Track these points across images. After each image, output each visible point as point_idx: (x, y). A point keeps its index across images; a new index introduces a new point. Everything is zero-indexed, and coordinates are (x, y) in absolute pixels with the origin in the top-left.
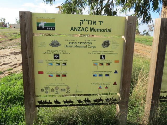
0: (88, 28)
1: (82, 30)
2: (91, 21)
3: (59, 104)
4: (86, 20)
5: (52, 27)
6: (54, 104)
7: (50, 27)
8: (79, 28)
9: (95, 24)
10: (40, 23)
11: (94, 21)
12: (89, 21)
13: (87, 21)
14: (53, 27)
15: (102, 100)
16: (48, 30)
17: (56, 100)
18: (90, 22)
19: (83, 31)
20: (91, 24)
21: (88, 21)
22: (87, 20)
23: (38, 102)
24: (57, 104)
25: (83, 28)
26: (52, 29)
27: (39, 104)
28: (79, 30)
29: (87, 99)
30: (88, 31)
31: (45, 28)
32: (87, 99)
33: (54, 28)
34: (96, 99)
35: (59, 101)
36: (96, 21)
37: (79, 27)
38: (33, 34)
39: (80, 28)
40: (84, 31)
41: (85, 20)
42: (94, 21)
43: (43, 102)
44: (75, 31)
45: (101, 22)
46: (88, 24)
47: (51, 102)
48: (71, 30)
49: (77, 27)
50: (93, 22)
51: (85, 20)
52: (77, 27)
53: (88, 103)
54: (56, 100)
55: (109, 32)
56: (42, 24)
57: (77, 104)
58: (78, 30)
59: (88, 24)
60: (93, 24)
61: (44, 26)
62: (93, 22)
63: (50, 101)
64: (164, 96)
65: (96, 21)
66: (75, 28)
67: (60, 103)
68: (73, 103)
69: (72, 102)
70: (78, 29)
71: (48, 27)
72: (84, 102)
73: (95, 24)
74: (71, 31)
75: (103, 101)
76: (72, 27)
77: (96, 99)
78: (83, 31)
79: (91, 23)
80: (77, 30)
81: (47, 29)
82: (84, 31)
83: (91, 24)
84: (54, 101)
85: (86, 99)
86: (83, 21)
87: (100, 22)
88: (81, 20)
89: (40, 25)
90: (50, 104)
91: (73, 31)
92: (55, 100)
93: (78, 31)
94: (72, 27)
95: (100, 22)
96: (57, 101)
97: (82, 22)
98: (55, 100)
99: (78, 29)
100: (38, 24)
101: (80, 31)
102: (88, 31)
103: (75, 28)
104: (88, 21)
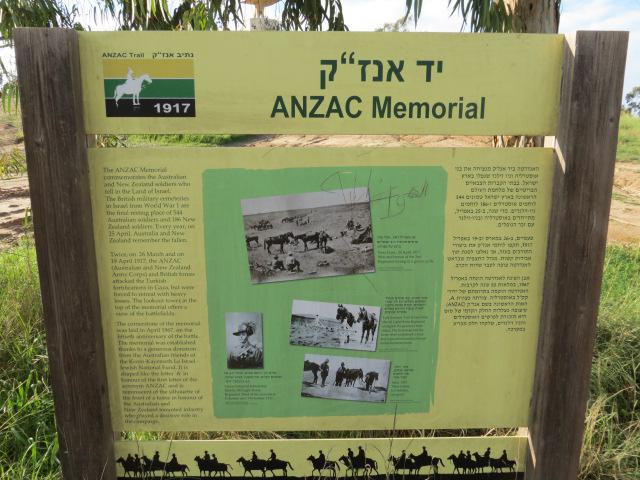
0: (359, 100)
1: (330, 110)
2: (376, 62)
3: (218, 475)
4: (352, 61)
5: (180, 102)
7: (172, 102)
9: (401, 79)
10: (123, 82)
12: (368, 62)
13: (356, 62)
16: (163, 114)
17: (207, 456)
20: (378, 79)
21: (360, 62)
22: (357, 58)
23: (121, 460)
24: (213, 474)
25: (334, 99)
26: (182, 108)
27: (127, 470)
29: (356, 453)
30: (359, 113)
32: (356, 453)
33: (188, 105)
34: (404, 455)
35: (219, 461)
36: (402, 63)
37: (312, 98)
39: (321, 99)
40: (341, 116)
41: (347, 57)
43: (473, 458)
44: (293, 115)
45: (429, 64)
47: (180, 462)
48: (275, 110)
49: (305, 98)
51: (344, 61)
52: (305, 98)
55: (475, 116)
56: (132, 88)
60: (389, 79)
62: (386, 68)
65: (402, 63)
66: (294, 100)
68: (288, 468)
69: (283, 465)
70: (311, 104)
71: (162, 102)
72: (342, 464)
73: (401, 79)
74: (273, 115)
76: (279, 99)
79: (376, 75)
80: (303, 114)
81: (153, 113)
82: (341, 116)
84: (197, 459)
86: (334, 63)
87: (425, 68)
88: (324, 62)
89: (119, 93)
91: (287, 115)
92: (202, 456)
93: (312, 115)
94: (279, 99)
95: (425, 68)
96: (212, 458)
97: (328, 69)
98: (202, 456)
99: (311, 104)
100: (110, 85)
101: (321, 116)
102: (359, 113)
103: (294, 100)
104: (360, 62)
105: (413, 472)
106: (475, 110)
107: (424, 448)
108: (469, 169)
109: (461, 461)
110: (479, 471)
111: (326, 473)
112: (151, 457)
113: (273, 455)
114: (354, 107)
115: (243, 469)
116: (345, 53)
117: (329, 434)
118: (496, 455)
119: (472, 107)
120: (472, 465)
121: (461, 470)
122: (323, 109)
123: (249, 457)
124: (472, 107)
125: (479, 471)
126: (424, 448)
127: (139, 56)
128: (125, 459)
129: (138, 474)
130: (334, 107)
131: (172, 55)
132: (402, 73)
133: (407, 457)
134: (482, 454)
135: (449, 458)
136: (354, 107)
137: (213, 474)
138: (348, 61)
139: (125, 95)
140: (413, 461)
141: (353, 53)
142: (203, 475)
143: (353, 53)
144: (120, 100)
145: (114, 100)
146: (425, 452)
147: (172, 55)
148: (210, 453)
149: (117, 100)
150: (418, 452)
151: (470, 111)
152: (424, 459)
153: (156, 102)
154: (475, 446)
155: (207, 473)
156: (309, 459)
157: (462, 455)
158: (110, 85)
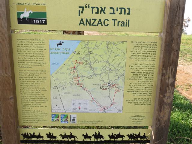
0: (108, 20)
1: (98, 24)
3: (53, 140)
4: (89, 7)
5: (42, 20)
6: (46, 138)
7: (39, 20)
8: (94, 20)
9: (104, 13)
10: (23, 13)
11: (101, 8)
12: (94, 7)
13: (90, 7)
14: (44, 19)
15: (122, 136)
16: (36, 24)
17: (50, 134)
18: (95, 10)
19: (100, 25)
20: (97, 13)
21: (91, 7)
22: (90, 6)
23: (22, 134)
24: (52, 139)
25: (100, 20)
26: (42, 22)
27: (24, 138)
28: (94, 24)
29: (97, 134)
30: (108, 24)
31: (30, 21)
32: (97, 134)
33: (44, 21)
34: (113, 134)
35: (54, 135)
36: (105, 8)
37: (93, 19)
38: (13, 31)
39: (95, 20)
40: (102, 25)
41: (87, 6)
42: (101, 8)
43: (135, 136)
44: (86, 25)
46: (92, 13)
47: (41, 135)
48: (80, 23)
49: (90, 19)
50: (100, 9)
51: (86, 7)
52: (90, 19)
53: (99, 140)
54: (50, 134)
55: (124, 26)
56: (26, 15)
57: (82, 140)
58: (91, 23)
59: (92, 13)
60: (101, 13)
61: (29, 17)
62: (100, 9)
63: (39, 134)
64: (139, 134)
65: (105, 8)
66: (87, 20)
67: (55, 137)
68: (76, 138)
69: (74, 137)
70: (92, 21)
71: (36, 20)
72: (93, 137)
73: (104, 13)
74: (80, 25)
75: (123, 138)
76: (82, 20)
77: (113, 134)
78: (100, 25)
79: (97, 12)
80: (90, 25)
81: (33, 23)
82: (102, 25)
83: (96, 13)
84: (47, 134)
85: (96, 133)
86: (83, 7)
88: (79, 7)
89: (22, 16)
90: (41, 139)
91: (84, 25)
92: (48, 134)
93: (93, 25)
94: (82, 20)
96: (51, 134)
97: (81, 9)
98: (48, 134)
99: (92, 21)
100: (19, 14)
101: (96, 25)
102: (108, 24)
103: (87, 20)
104: (91, 7)
105: (116, 140)
106: (124, 24)
107: (119, 132)
108: (21, 40)
109: (131, 136)
110: (136, 139)
111: (88, 140)
112: (32, 134)
113: (71, 134)
114: (106, 22)
115: (23, 138)
116: (86, 4)
117: (88, 127)
118: (142, 135)
119: (123, 23)
120: (29, 137)
121: (131, 139)
122: (96, 23)
123: (63, 134)
124: (123, 23)
125: (136, 139)
126: (119, 132)
127: (28, 4)
128: (24, 134)
129: (133, 139)
130: (100, 22)
131: (39, 4)
132: (105, 11)
133: (114, 135)
134: (137, 134)
135: (127, 136)
136: (106, 22)
137: (52, 139)
138: (87, 7)
139: (24, 17)
140: (116, 136)
141: (89, 4)
142: (49, 140)
143: (89, 4)
144: (22, 19)
145: (20, 19)
146: (119, 133)
147: (39, 4)
148: (51, 133)
149: (21, 19)
150: (117, 133)
151: (122, 24)
152: (119, 136)
153: (34, 19)
154: (135, 132)
155: (50, 139)
156: (108, 136)
157: (131, 134)
158: (19, 14)
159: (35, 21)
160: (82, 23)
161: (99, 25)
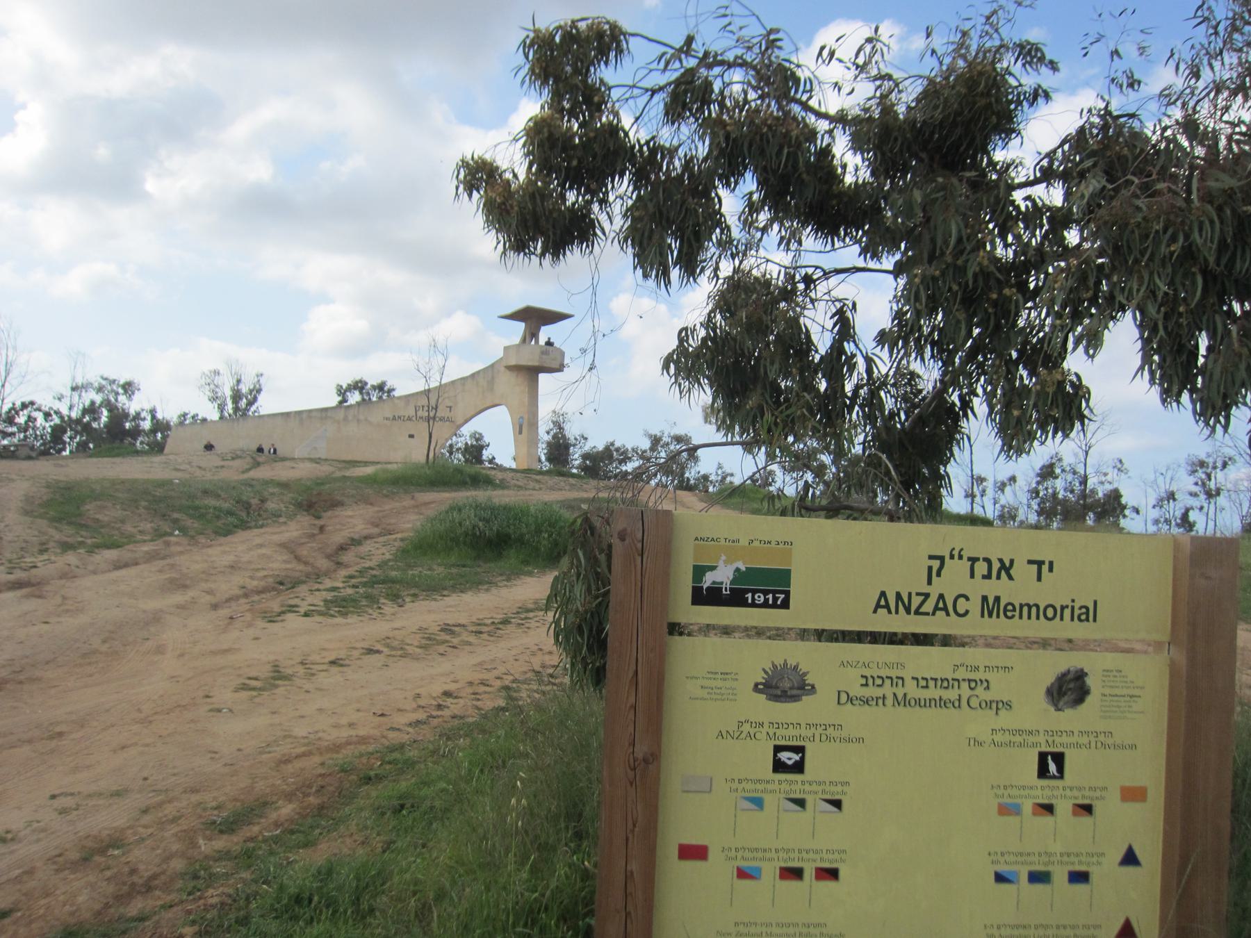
0: (967, 599)
1: (936, 608)
4: (960, 557)
5: (774, 592)
7: (765, 593)
9: (1010, 578)
10: (713, 568)
11: (1001, 561)
12: (978, 559)
13: (965, 558)
16: (754, 605)
18: (981, 568)
19: (940, 614)
20: (988, 577)
21: (969, 559)
22: (965, 554)
25: (941, 597)
26: (775, 599)
30: (967, 612)
36: (1012, 561)
37: (918, 594)
39: (927, 596)
40: (948, 614)
41: (956, 553)
42: (1001, 561)
44: (897, 612)
46: (972, 576)
48: (878, 606)
49: (910, 594)
50: (996, 566)
51: (952, 557)
52: (910, 594)
55: (1087, 620)
56: (722, 575)
58: (913, 608)
59: (972, 576)
60: (998, 577)
62: (996, 566)
65: (1012, 561)
70: (916, 601)
71: (754, 592)
73: (1010, 578)
74: (875, 611)
76: (883, 594)
78: (940, 614)
80: (908, 611)
82: (948, 614)
88: (931, 557)
89: (708, 580)
91: (890, 612)
93: (917, 612)
94: (883, 594)
97: (936, 564)
99: (916, 601)
100: (699, 572)
101: (927, 614)
102: (967, 612)
104: (969, 559)
119: (1084, 610)
122: (929, 606)
124: (1084, 610)
130: (941, 605)
132: (1012, 572)
136: (962, 605)
138: (956, 557)
139: (714, 583)
144: (708, 588)
153: (748, 591)
158: (699, 572)
159: (749, 595)
160: (941, 609)
161: (938, 613)
